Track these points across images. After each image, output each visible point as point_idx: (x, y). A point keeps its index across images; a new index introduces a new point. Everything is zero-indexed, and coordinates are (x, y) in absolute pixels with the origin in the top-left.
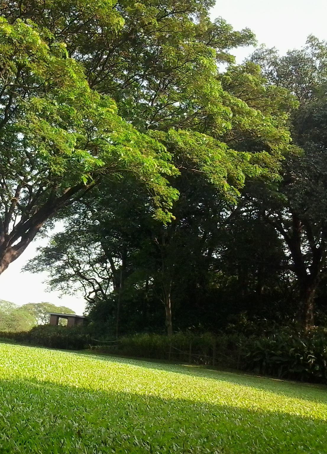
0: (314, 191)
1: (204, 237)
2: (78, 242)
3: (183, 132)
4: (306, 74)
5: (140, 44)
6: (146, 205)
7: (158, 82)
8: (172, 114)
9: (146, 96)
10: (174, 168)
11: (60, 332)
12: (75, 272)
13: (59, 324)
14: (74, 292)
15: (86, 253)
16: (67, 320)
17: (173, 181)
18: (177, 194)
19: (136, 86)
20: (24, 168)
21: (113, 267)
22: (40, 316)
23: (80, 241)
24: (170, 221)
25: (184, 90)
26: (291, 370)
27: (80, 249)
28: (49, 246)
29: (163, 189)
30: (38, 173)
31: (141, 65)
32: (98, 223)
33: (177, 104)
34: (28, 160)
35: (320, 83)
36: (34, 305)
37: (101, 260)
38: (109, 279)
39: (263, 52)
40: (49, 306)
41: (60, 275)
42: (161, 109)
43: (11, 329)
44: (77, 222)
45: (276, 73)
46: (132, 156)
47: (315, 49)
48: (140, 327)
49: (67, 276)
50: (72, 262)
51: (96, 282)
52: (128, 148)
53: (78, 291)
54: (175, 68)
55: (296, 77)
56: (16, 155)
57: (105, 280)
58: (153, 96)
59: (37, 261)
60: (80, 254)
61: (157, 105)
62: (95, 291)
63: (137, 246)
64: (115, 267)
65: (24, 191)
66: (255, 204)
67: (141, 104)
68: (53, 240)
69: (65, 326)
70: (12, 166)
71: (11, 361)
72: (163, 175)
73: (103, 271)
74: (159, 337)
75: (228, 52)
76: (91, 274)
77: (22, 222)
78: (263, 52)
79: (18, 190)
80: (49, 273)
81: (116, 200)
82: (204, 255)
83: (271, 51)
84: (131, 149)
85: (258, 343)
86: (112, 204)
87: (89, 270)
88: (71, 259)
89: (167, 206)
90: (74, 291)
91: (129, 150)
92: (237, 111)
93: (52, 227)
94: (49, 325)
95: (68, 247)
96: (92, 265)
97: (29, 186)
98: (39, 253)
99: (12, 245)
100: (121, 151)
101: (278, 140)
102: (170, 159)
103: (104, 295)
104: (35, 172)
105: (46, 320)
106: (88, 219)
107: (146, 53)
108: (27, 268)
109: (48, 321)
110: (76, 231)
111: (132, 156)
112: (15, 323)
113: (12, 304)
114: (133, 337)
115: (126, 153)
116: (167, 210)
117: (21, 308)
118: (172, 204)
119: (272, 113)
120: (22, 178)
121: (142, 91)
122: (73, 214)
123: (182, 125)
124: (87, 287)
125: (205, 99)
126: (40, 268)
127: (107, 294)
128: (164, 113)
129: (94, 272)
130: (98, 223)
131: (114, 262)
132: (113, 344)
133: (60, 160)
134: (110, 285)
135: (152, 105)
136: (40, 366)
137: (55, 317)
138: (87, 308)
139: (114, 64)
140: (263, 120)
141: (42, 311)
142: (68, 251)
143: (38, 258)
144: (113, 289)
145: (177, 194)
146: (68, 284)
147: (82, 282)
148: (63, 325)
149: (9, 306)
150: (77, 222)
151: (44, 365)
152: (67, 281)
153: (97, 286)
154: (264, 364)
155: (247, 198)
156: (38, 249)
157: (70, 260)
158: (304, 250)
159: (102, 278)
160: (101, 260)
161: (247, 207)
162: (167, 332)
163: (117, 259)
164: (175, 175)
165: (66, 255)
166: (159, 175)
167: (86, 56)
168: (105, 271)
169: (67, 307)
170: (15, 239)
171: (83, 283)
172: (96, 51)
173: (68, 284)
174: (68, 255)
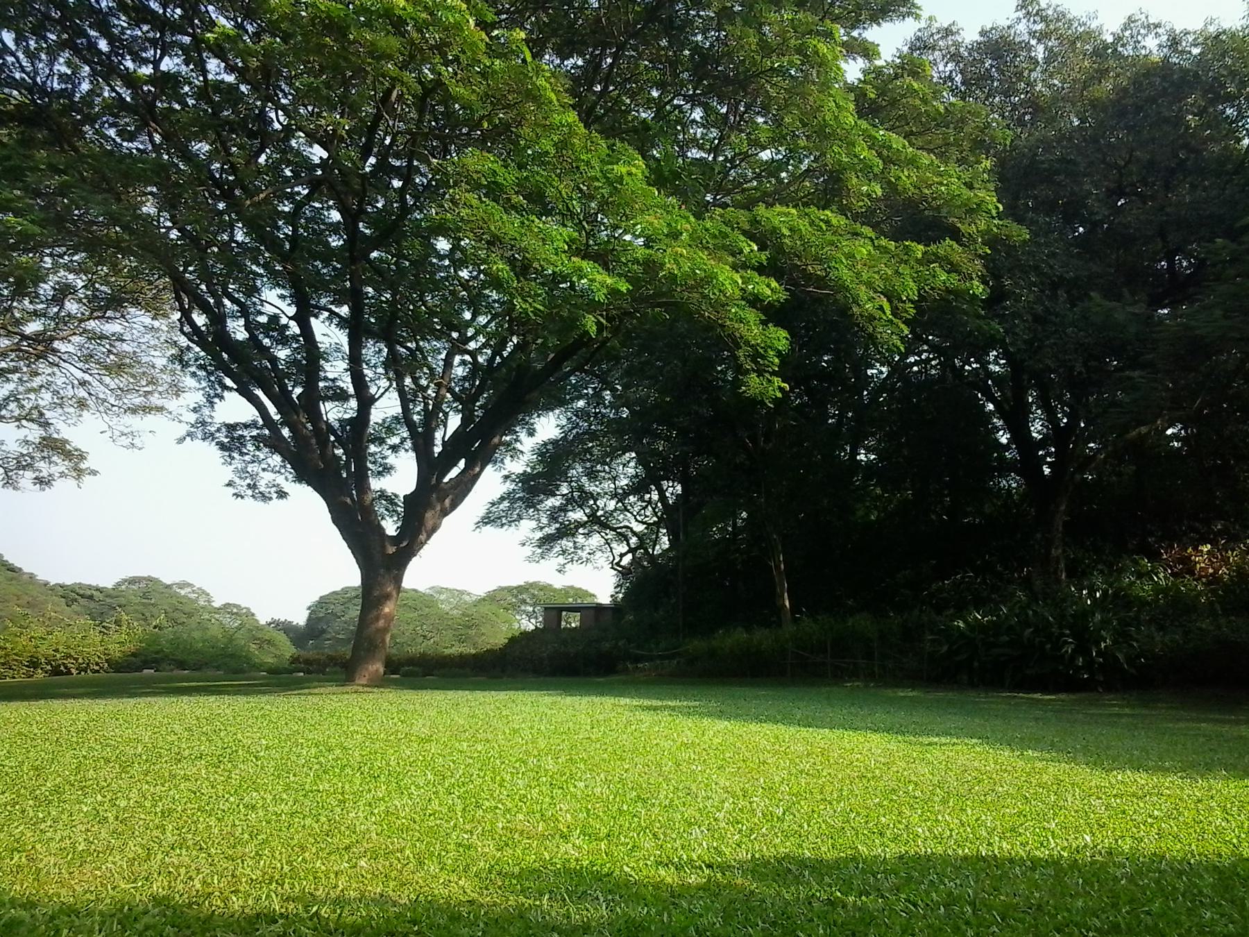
5: (681, 29)
7: (724, 110)
10: (774, 284)
14: (589, 556)
15: (607, 476)
17: (773, 314)
19: (678, 122)
22: (524, 611)
24: (779, 395)
33: (765, 155)
36: (509, 590)
37: (638, 488)
39: (932, 35)
41: (558, 525)
44: (581, 414)
45: (959, 75)
47: (1035, 22)
49: (572, 526)
53: (599, 554)
54: (758, 75)
59: (506, 504)
61: (726, 160)
65: (463, 363)
70: (432, 313)
72: (754, 301)
73: (644, 508)
78: (932, 35)
79: (448, 363)
83: (948, 32)
85: (961, 624)
89: (769, 366)
98: (509, 486)
99: (446, 480)
101: (972, 211)
104: (482, 320)
105: (536, 618)
107: (696, 48)
108: (487, 520)
116: (767, 375)
117: (484, 599)
118: (777, 361)
120: (455, 335)
125: (823, 134)
130: (625, 413)
137: (554, 612)
141: (528, 600)
152: (573, 535)
154: (976, 664)
158: (1037, 429)
159: (644, 523)
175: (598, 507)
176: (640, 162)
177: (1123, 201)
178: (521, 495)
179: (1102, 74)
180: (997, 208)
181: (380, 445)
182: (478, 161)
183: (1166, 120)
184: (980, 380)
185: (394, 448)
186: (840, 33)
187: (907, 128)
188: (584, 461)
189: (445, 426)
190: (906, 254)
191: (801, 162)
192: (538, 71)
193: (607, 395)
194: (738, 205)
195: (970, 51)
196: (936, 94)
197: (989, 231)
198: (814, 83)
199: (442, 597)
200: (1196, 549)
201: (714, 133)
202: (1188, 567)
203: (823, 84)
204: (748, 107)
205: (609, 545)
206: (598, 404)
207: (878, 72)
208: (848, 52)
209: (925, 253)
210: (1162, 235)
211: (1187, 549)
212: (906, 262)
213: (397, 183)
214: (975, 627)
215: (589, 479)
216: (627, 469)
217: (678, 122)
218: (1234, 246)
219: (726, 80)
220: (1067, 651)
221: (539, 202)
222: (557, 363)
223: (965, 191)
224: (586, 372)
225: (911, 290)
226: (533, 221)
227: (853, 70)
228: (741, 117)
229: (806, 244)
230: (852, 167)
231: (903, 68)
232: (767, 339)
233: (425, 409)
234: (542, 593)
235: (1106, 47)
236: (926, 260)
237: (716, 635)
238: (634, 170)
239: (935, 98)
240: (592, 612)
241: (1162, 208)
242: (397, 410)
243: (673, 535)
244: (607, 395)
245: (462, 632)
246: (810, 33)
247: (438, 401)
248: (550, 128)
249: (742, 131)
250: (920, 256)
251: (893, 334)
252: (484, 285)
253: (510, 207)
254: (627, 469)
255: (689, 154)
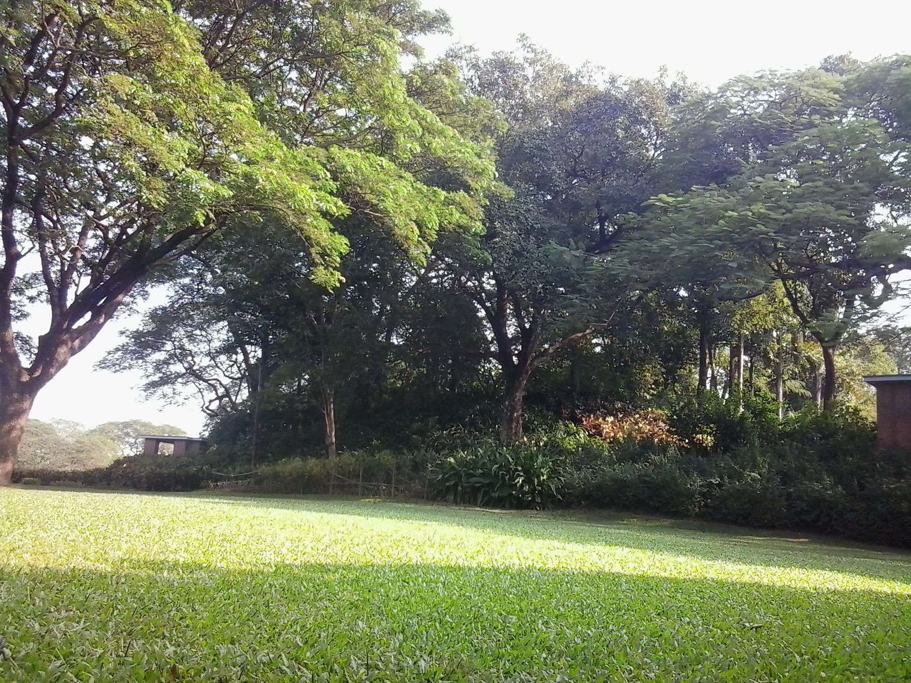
0: (524, 251)
1: (381, 314)
2: (190, 322)
3: (352, 152)
4: (516, 85)
5: (285, 12)
6: (296, 265)
7: (313, 75)
8: (335, 126)
9: (295, 95)
10: (340, 203)
11: (160, 466)
12: (187, 369)
13: (159, 453)
14: (184, 401)
15: (204, 339)
16: (172, 446)
17: (339, 225)
18: (346, 244)
19: (279, 78)
20: (93, 197)
21: (246, 360)
22: (128, 442)
23: (193, 320)
24: (338, 285)
25: (352, 91)
26: (493, 495)
27: (194, 332)
28: (141, 329)
29: (325, 236)
30: (119, 206)
31: (286, 45)
32: (222, 291)
33: (341, 112)
34: (100, 183)
35: (533, 100)
36: (116, 425)
37: (228, 349)
38: (241, 379)
39: (461, 49)
40: (143, 426)
41: (161, 375)
42: (318, 117)
43: (76, 465)
44: (187, 289)
45: (477, 80)
46: (277, 183)
47: (528, 52)
48: (288, 450)
49: (173, 376)
50: (180, 353)
51: (221, 384)
52: (270, 170)
53: (192, 399)
54: (340, 54)
55: (504, 88)
56: (78, 175)
57: (235, 381)
58: (306, 97)
59: (120, 353)
60: (194, 341)
61: (312, 111)
62: (219, 398)
63: (284, 327)
64: (251, 359)
65: (95, 236)
66: (449, 267)
67: (288, 107)
68: (147, 318)
69: (169, 455)
70: (72, 193)
71: (65, 525)
72: (325, 214)
73: (232, 366)
74: (317, 462)
75: (415, 40)
76: (212, 372)
77: (91, 287)
78: (461, 49)
79: (83, 234)
80: (142, 372)
81: (250, 256)
82: (380, 339)
83: (471, 49)
84: (275, 173)
85: (452, 460)
86: (244, 261)
87: (208, 366)
88: (179, 348)
89: (332, 263)
90: (185, 399)
91: (272, 173)
92: (428, 129)
93: (145, 295)
94: (143, 456)
95: (173, 330)
96: (213, 358)
97: (103, 226)
98: (124, 340)
99: (75, 327)
100: (260, 173)
101: (479, 174)
102: (335, 191)
103: (234, 403)
104: (114, 204)
105: (137, 448)
106: (206, 285)
107: (295, 28)
108: (103, 364)
109: (141, 449)
110: (186, 304)
111: (277, 183)
112: (83, 456)
113: (78, 424)
114: (278, 464)
115: (267, 177)
116: (331, 269)
117: (95, 430)
118: (338, 259)
119: (471, 138)
120: (90, 213)
121: (289, 87)
122: (181, 277)
123: (349, 141)
124: (205, 393)
125: (383, 105)
126: (127, 365)
127: (237, 402)
128: (322, 124)
129: (217, 369)
130: (222, 291)
131: (249, 352)
132: (246, 477)
133: (159, 183)
134: (242, 387)
135: (304, 110)
136: (118, 528)
137: (153, 442)
138: (206, 425)
139: (245, 40)
140: (461, 145)
141: (131, 433)
142: (174, 336)
143: (123, 348)
144: (247, 394)
145: (346, 244)
146: (174, 389)
147: (197, 384)
148: (167, 454)
149: (73, 429)
150: (188, 289)
151: (127, 524)
152: (173, 383)
153: (221, 391)
154: (460, 488)
155: (439, 258)
156: (122, 333)
157: (178, 351)
158: (511, 331)
159: (230, 378)
160: (228, 349)
161: (438, 271)
162: (327, 453)
163: (253, 347)
164: (343, 215)
165: (170, 342)
166: (319, 214)
167: (198, 21)
168: (235, 366)
169: (172, 425)
170: (81, 315)
171: (200, 387)
172: (216, 16)
173: (174, 389)
174: (173, 342)
175: (195, 362)
176: (249, 102)
177: (576, 181)
178: (133, 348)
179: (567, 94)
180: (495, 175)
181: (20, 294)
182: (125, 84)
183: (606, 131)
184: (476, 294)
185: (31, 299)
186: (398, 35)
187: (440, 110)
188: (185, 325)
189: (77, 285)
190: (434, 196)
191: (366, 121)
192: (176, 21)
193: (209, 277)
194: (320, 145)
195: (485, 64)
196: (461, 90)
197: (489, 189)
198: (379, 67)
199: (60, 426)
200: (604, 419)
201: (305, 90)
202: (598, 431)
203: (385, 69)
204: (331, 76)
205: (201, 392)
206: (201, 283)
207: (424, 68)
208: (403, 50)
209: (446, 197)
210: (598, 206)
211: (598, 419)
212: (433, 202)
213: (51, 90)
214: (462, 463)
215: (189, 340)
216: (220, 333)
217: (279, 78)
218: (639, 218)
219: (317, 54)
220: (519, 482)
221: (168, 119)
222: (173, 243)
223: (475, 159)
224: (193, 256)
225: (433, 223)
226: (163, 133)
227: (406, 63)
228: (326, 81)
229: (366, 180)
230: (401, 130)
231: (441, 68)
232: (333, 243)
233: (62, 270)
234: (143, 429)
235: (571, 76)
236: (448, 203)
237: (280, 462)
238: (242, 107)
239: (461, 92)
240: (184, 443)
241: (599, 188)
242: (38, 267)
243: (253, 387)
244: (209, 277)
245: (75, 455)
246: (379, 32)
247: (72, 267)
248: (181, 64)
249: (325, 92)
250: (443, 198)
251: (420, 252)
252: (118, 178)
253: (144, 120)
254: (220, 333)
255: (285, 103)
